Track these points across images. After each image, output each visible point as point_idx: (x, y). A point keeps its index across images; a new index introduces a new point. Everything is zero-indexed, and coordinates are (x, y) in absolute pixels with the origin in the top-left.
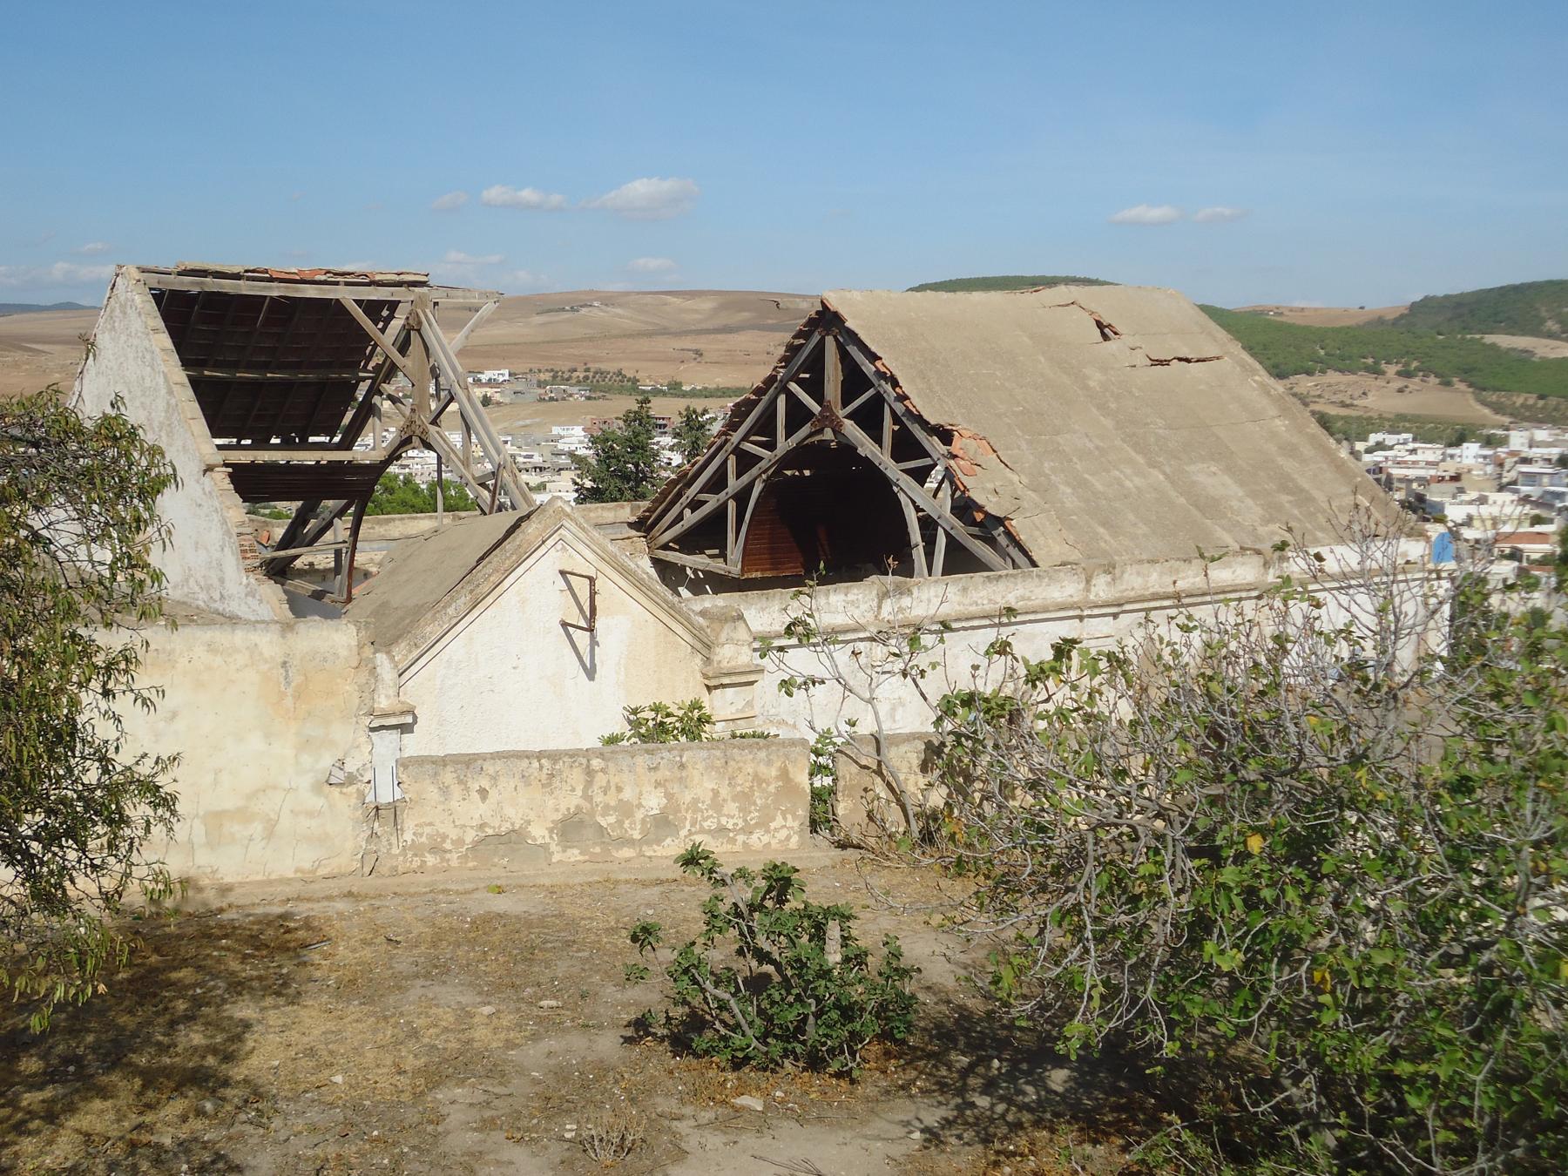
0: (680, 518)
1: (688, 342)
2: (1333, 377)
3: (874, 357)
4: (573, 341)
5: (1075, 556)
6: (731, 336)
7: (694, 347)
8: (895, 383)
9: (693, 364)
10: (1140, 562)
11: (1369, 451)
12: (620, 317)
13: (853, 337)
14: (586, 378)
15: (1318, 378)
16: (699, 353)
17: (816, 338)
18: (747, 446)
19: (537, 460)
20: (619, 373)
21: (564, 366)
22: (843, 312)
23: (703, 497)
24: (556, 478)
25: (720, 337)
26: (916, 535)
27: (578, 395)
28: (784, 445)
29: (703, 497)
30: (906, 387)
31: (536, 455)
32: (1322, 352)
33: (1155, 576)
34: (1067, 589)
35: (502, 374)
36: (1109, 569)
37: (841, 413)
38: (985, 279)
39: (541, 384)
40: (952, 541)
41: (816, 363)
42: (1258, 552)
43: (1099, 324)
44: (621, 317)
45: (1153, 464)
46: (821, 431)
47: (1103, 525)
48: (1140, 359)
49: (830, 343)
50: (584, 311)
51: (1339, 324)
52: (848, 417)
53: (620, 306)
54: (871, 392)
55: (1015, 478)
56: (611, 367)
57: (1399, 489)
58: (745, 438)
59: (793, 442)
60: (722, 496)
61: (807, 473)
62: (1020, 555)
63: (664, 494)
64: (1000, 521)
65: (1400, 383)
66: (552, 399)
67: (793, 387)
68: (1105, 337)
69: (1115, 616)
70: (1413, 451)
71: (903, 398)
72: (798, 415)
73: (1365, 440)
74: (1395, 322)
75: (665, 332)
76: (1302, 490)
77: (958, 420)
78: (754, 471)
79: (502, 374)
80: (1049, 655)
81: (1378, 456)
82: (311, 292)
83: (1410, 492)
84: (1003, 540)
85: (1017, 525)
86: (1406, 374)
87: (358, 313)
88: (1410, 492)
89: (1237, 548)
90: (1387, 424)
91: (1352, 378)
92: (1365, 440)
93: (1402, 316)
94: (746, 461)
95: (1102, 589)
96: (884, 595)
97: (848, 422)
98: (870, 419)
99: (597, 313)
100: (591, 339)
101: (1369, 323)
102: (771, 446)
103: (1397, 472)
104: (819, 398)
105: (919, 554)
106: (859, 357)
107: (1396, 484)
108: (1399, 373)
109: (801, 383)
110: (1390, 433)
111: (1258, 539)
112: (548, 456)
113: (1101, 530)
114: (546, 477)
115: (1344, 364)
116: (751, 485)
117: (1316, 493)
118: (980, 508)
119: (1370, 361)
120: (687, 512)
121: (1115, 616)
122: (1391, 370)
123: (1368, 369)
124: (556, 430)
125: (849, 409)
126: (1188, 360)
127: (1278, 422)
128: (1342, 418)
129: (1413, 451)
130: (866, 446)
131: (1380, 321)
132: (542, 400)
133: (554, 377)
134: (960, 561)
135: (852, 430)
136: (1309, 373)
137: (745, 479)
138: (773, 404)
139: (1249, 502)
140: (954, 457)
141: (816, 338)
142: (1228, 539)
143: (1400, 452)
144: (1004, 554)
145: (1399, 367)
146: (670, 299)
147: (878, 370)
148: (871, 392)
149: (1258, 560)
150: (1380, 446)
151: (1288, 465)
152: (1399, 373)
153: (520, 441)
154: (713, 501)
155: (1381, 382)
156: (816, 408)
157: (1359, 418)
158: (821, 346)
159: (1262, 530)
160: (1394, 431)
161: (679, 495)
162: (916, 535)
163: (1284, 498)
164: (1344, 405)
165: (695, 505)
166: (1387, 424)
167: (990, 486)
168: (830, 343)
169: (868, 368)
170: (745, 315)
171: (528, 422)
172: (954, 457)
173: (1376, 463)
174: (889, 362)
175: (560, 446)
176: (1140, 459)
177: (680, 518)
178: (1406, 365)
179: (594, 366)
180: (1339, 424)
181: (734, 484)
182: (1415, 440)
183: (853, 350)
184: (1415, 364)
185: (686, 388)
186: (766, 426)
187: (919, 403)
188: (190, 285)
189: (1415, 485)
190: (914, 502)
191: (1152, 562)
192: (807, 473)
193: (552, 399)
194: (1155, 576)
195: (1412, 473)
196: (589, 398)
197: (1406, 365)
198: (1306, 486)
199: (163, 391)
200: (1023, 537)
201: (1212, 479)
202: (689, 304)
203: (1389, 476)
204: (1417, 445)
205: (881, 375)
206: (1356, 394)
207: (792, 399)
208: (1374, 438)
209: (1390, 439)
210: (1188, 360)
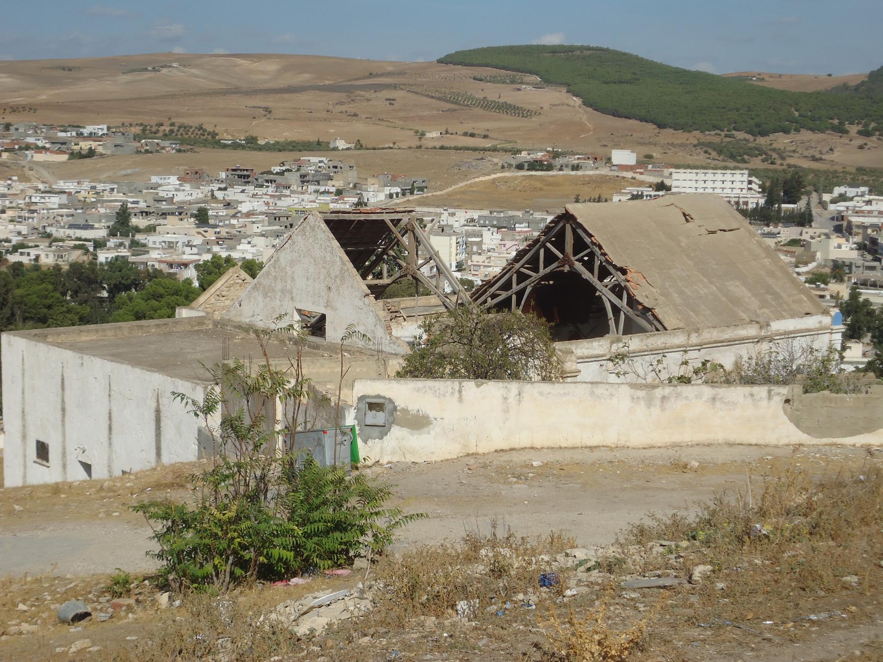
0: (485, 302)
1: (259, 101)
2: (806, 135)
3: (590, 236)
4: (158, 98)
5: (681, 325)
6: (294, 96)
7: (263, 104)
8: (600, 248)
9: (264, 120)
10: (709, 327)
11: (834, 201)
12: (196, 76)
13: (581, 226)
14: (172, 131)
15: (793, 136)
16: (268, 110)
17: (561, 224)
18: (523, 270)
19: (142, 205)
20: (200, 128)
21: (152, 120)
22: (576, 214)
23: (499, 292)
24: (161, 221)
25: (286, 96)
26: (610, 315)
27: (169, 148)
28: (542, 271)
29: (499, 292)
30: (606, 249)
31: (141, 200)
32: (797, 114)
33: (715, 333)
34: (679, 339)
35: (100, 129)
36: (697, 330)
37: (573, 259)
38: (512, 47)
39: (137, 138)
40: (627, 318)
41: (561, 235)
42: (758, 322)
43: (685, 215)
44: (198, 77)
45: (711, 282)
46: (563, 266)
47: (692, 311)
48: (703, 231)
49: (568, 227)
50: (164, 71)
51: (810, 90)
52: (577, 260)
53: (196, 66)
54: (589, 250)
55: (654, 290)
56: (194, 122)
57: (857, 234)
58: (522, 266)
59: (548, 270)
60: (510, 292)
61: (551, 282)
62: (659, 326)
63: (477, 291)
64: (649, 310)
65: (860, 141)
66: (147, 151)
67: (549, 245)
68: (687, 221)
69: (699, 350)
70: (869, 202)
71: (605, 254)
72: (550, 258)
73: (831, 192)
74: (857, 88)
75: (237, 91)
76: (776, 293)
77: (629, 264)
78: (527, 282)
79: (100, 129)
80: (700, 365)
81: (841, 206)
82: (374, 217)
83: (866, 236)
84: (651, 318)
85: (657, 311)
86: (865, 133)
87: (390, 224)
88: (866, 236)
89: (748, 320)
90: (849, 177)
91: (821, 136)
92: (831, 192)
93: (863, 83)
94: (522, 277)
95: (694, 339)
96: (612, 343)
97: (577, 263)
98: (589, 266)
99: (175, 73)
100: (173, 96)
101: (836, 89)
102: (536, 270)
103: (855, 220)
104: (562, 251)
105: (612, 323)
106: (583, 235)
107: (855, 230)
108: (860, 133)
109: (552, 243)
110: (851, 186)
111: (757, 316)
112: (151, 202)
113: (691, 313)
114: (152, 221)
115: (814, 123)
116: (525, 289)
117: (782, 294)
118: (640, 304)
119: (836, 122)
120: (489, 299)
121: (699, 350)
122: (854, 129)
123: (834, 129)
124: (155, 179)
125: (577, 257)
126: (725, 231)
127: (766, 260)
128: (813, 171)
129: (869, 202)
130: (586, 275)
131: (845, 87)
132: (138, 152)
133: (144, 130)
134: (631, 328)
135: (579, 266)
136: (786, 131)
137: (522, 285)
138: (537, 254)
139: (753, 298)
140: (628, 281)
141: (561, 224)
142: (744, 316)
143: (858, 203)
144: (651, 323)
145: (860, 128)
146: (240, 61)
147: (592, 242)
148: (589, 250)
149: (757, 326)
150: (843, 198)
151: (770, 281)
152: (860, 133)
153: (125, 189)
154: (504, 295)
155: (844, 140)
156: (561, 256)
157: (825, 172)
158: (564, 227)
159: (759, 312)
160: (853, 184)
161: (485, 291)
162: (610, 315)
163: (769, 297)
164: (814, 159)
165: (493, 296)
166: (849, 177)
167: (644, 294)
168: (568, 228)
169: (587, 240)
170: (306, 76)
171: (129, 171)
172: (628, 281)
173: (840, 212)
174: (598, 238)
175: (162, 194)
176: (706, 280)
177: (485, 302)
178: (866, 125)
179: (178, 121)
180: (810, 177)
181: (515, 288)
182: (871, 192)
183: (580, 231)
184: (873, 125)
185: (261, 142)
186: (534, 264)
187: (612, 257)
188: (333, 217)
189: (869, 231)
190: (610, 301)
191: (714, 327)
192: (551, 282)
193: (147, 151)
194: (715, 333)
195: (867, 221)
196: (179, 151)
197: (866, 125)
198: (778, 291)
199: (339, 263)
200: (660, 317)
201: (738, 289)
202: (256, 66)
203: (850, 222)
204: (871, 197)
205: (595, 244)
206: (825, 150)
207: (547, 250)
208: (837, 191)
209: (851, 192)
210: (725, 231)
